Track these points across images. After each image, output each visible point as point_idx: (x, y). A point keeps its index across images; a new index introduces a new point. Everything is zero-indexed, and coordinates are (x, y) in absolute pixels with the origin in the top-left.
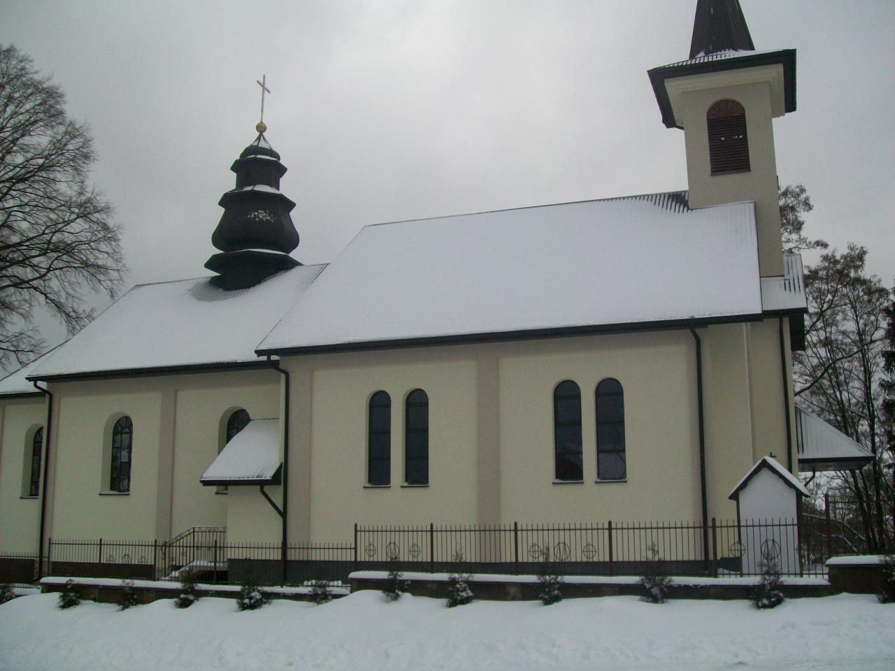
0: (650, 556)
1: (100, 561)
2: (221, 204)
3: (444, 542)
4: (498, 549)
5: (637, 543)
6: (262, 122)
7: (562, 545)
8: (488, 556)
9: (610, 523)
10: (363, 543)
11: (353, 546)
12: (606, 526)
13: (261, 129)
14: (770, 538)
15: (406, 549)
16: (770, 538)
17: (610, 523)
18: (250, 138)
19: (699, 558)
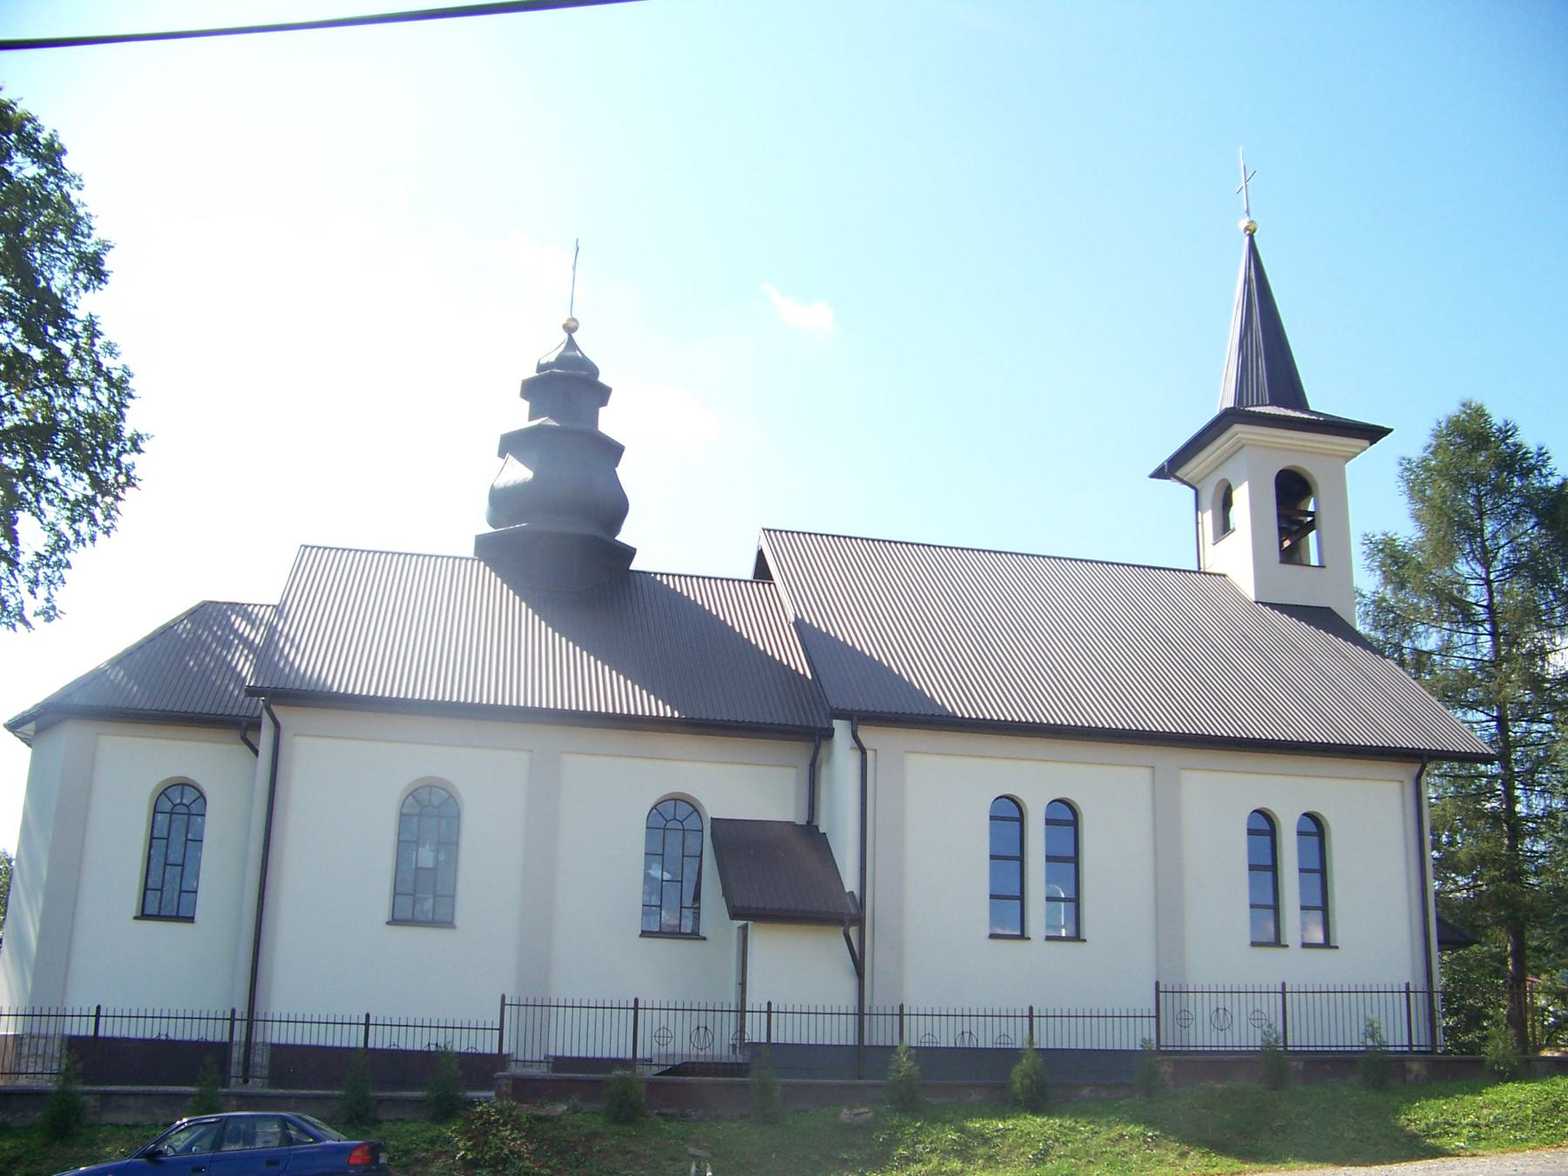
0: (1369, 1042)
1: (1031, 1041)
2: (530, 389)
3: (607, 1026)
4: (545, 1030)
5: (607, 1035)
6: (571, 344)
7: (702, 1031)
8: (820, 1034)
9: (1031, 1009)
10: (1170, 1009)
11: (1153, 1013)
12: (1026, 1013)
13: (570, 328)
14: (966, 1029)
15: (1243, 1019)
16: (966, 1029)
17: (1031, 1009)
18: (550, 348)
19: (851, 1042)
